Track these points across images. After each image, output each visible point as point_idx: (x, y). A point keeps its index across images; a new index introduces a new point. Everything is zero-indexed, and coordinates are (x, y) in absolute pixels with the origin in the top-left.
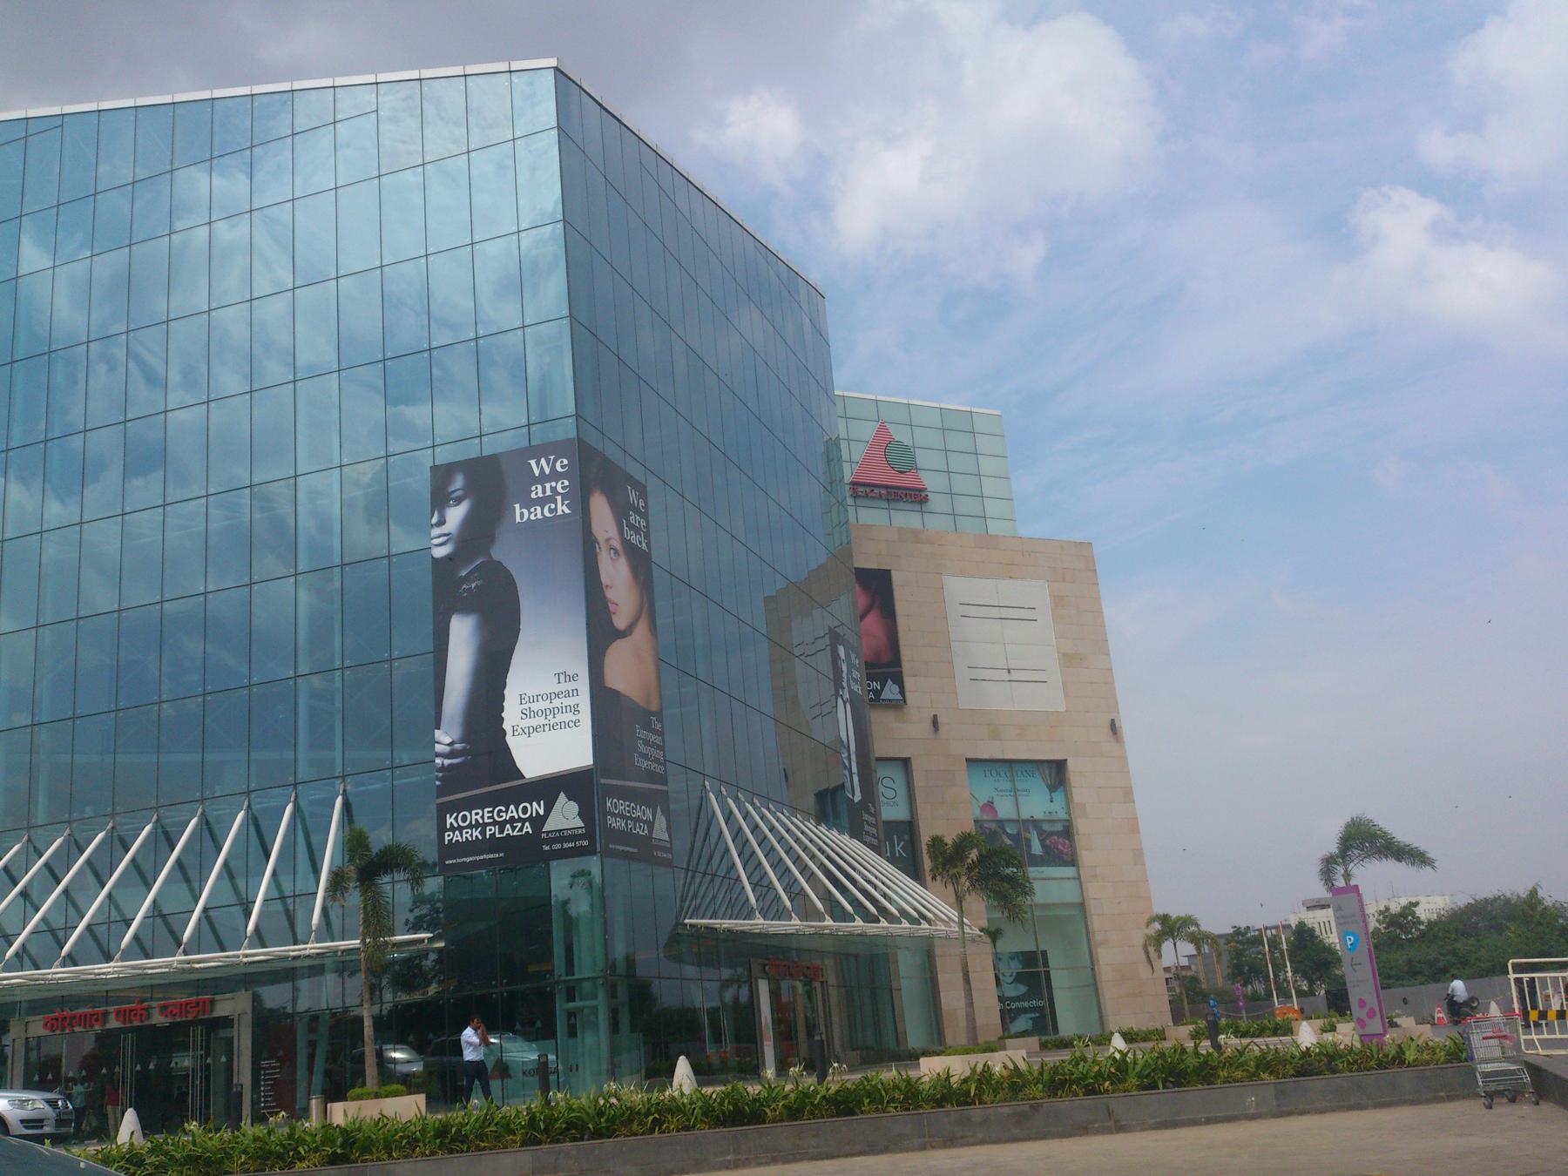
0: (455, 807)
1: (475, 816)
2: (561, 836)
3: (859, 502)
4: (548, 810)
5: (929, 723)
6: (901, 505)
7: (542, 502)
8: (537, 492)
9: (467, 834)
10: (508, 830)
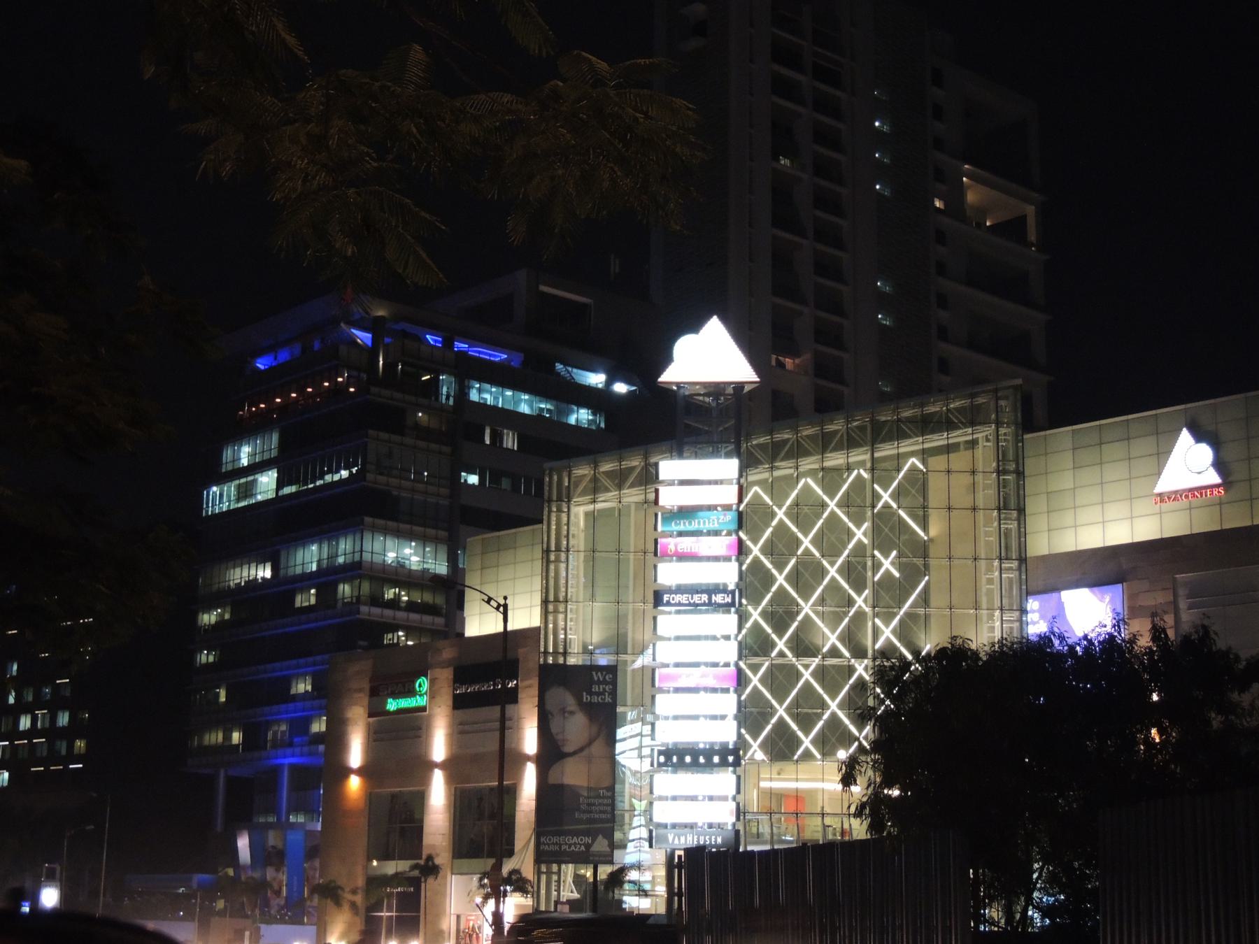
4: (593, 841)
7: (598, 694)
8: (595, 688)
10: (573, 848)
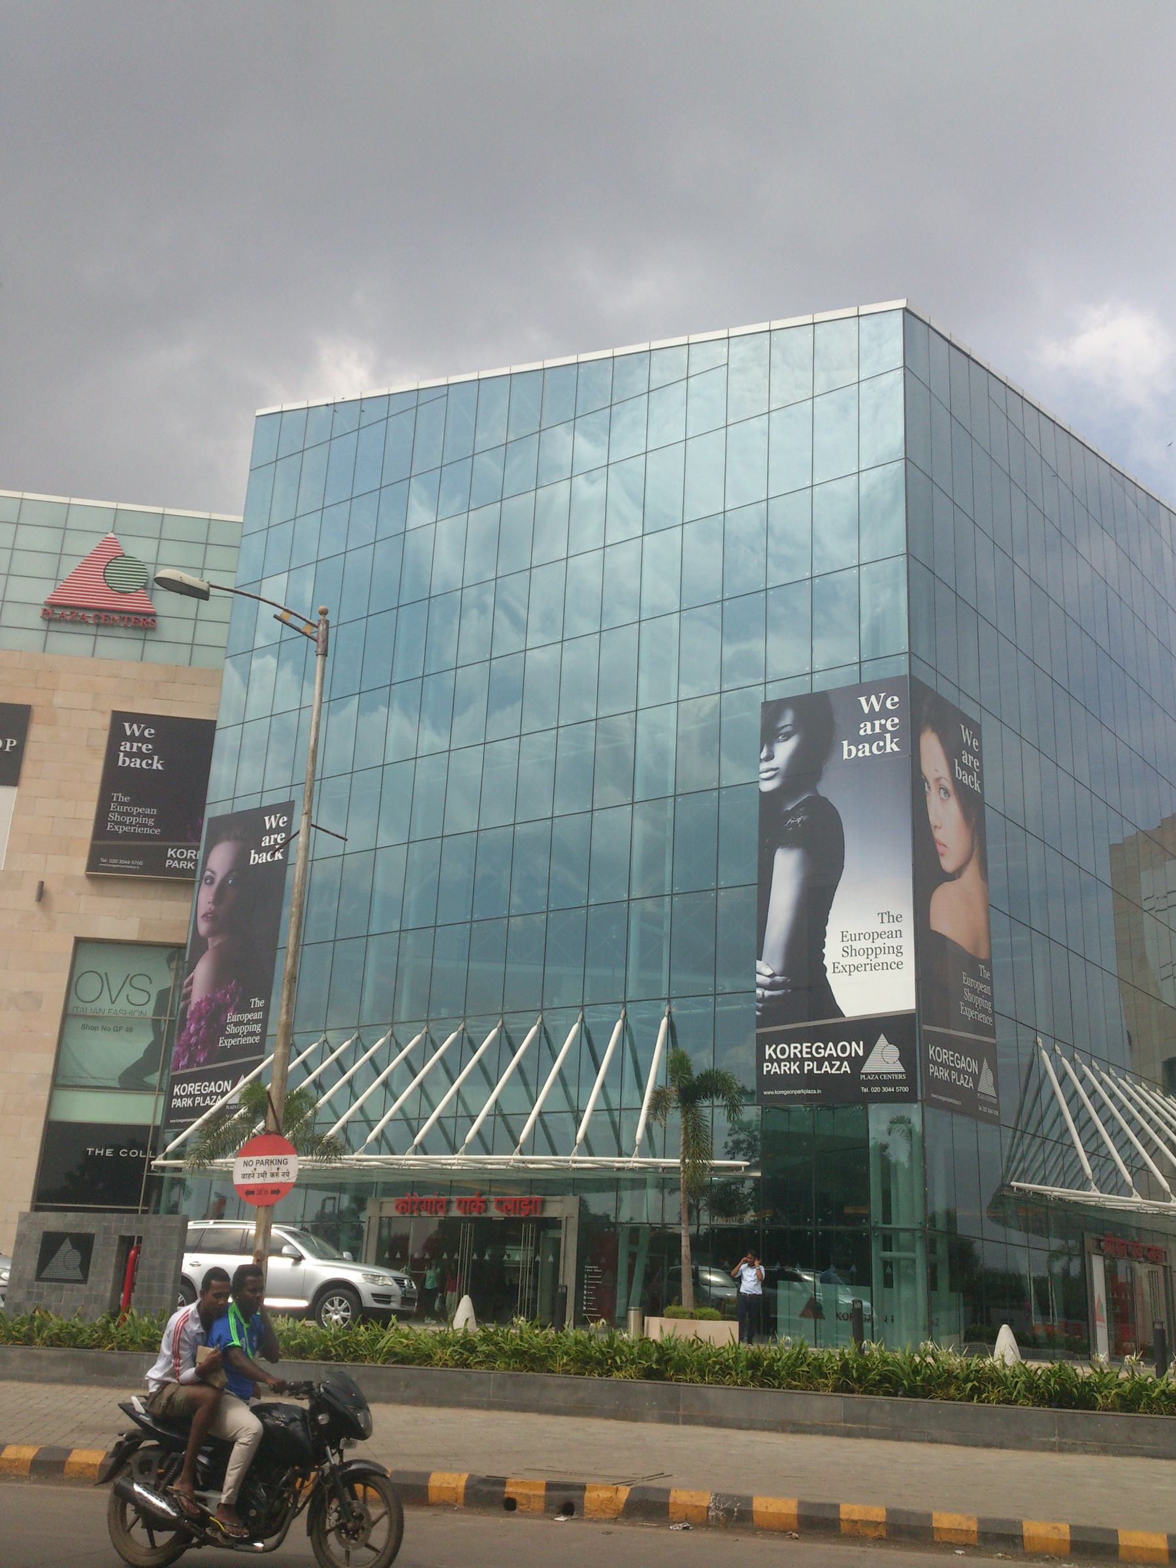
0: (774, 1039)
1: (794, 1049)
2: (880, 1080)
3: (53, 627)
4: (868, 1050)
5: (34, 893)
6: (120, 632)
7: (870, 739)
9: (785, 1067)
